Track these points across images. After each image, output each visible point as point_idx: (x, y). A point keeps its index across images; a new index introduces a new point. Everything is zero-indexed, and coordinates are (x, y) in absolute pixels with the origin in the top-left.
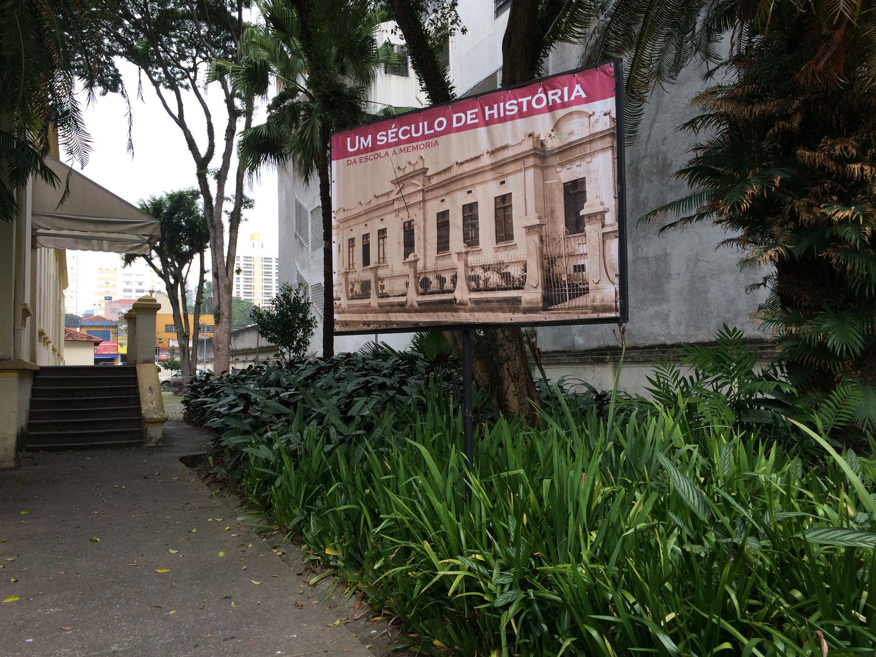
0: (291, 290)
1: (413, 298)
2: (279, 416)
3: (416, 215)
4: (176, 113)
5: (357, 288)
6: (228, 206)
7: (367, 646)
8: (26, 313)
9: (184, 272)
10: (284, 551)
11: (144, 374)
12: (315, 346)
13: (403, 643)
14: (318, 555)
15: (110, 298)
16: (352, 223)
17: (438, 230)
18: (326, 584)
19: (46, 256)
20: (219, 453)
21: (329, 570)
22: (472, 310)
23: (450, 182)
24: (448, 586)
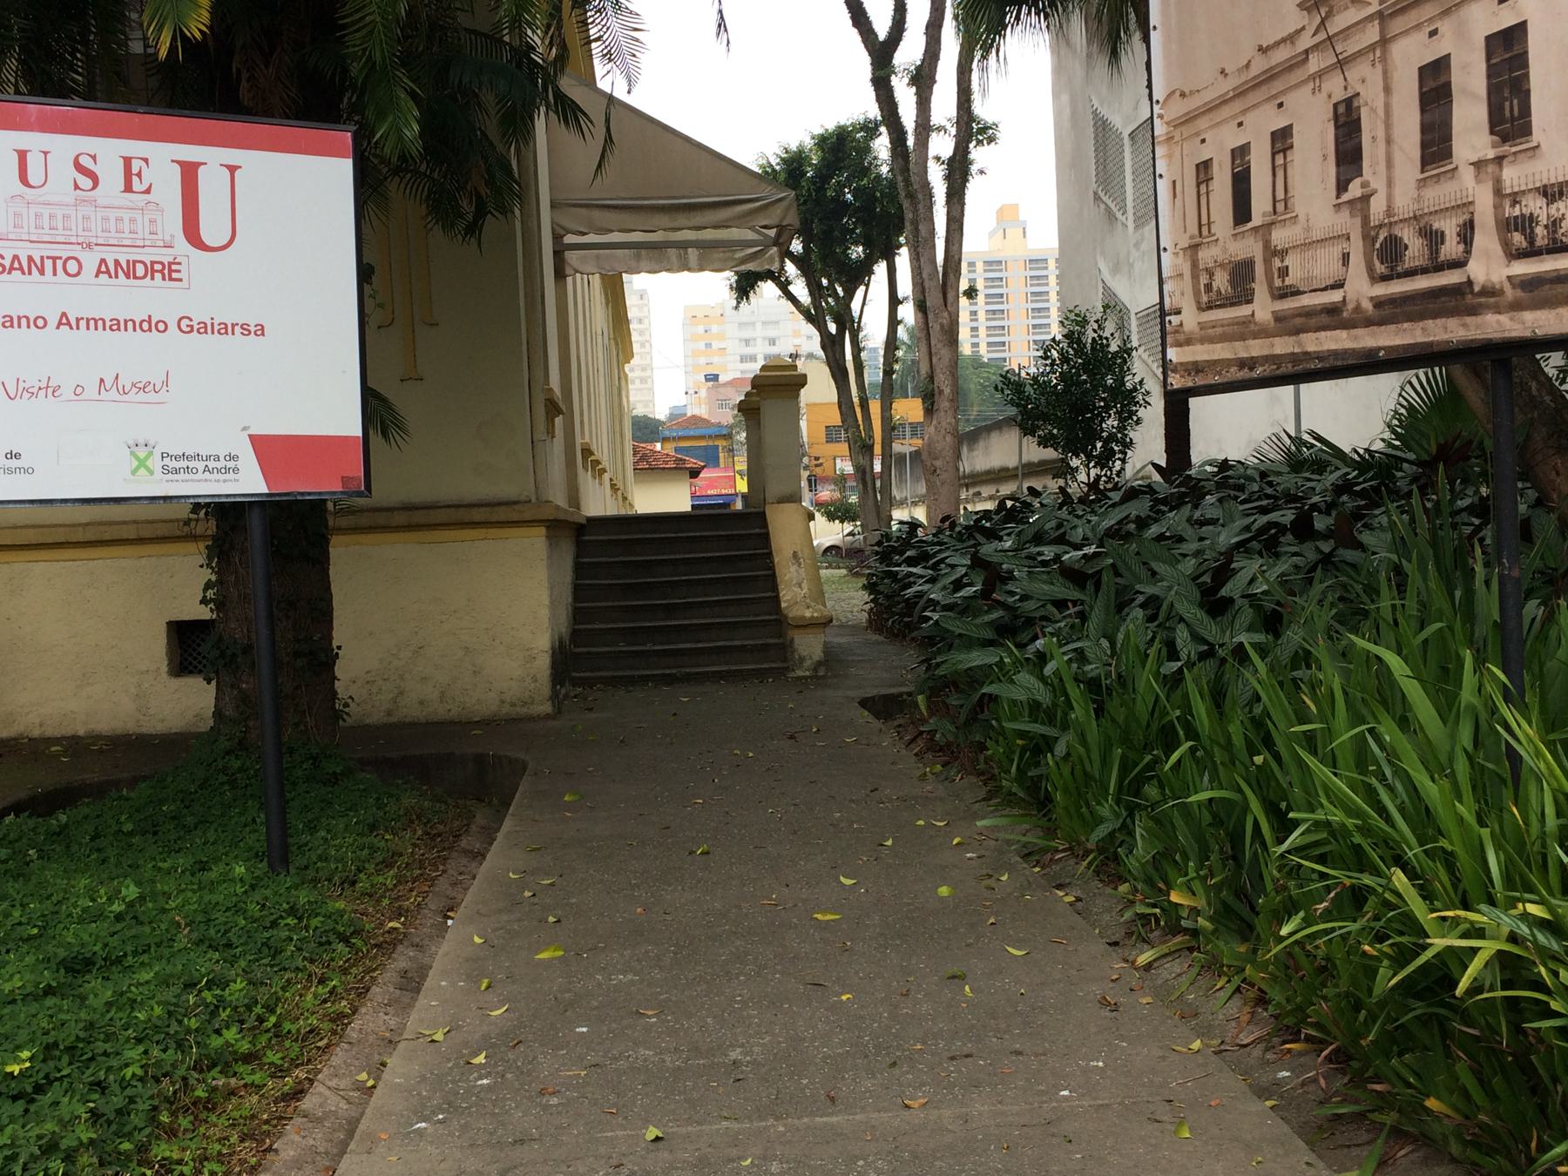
0: (1084, 322)
1: (1361, 290)
2: (1061, 604)
3: (1365, 81)
4: (882, 28)
5: (1221, 281)
6: (942, 145)
7: (1269, 1103)
8: (553, 409)
9: (856, 305)
10: (1079, 893)
11: (781, 522)
12: (1148, 445)
13: (1356, 1102)
14: (1154, 906)
15: (715, 378)
16: (1203, 123)
17: (1423, 111)
18: (1175, 966)
19: (586, 291)
20: (939, 687)
21: (1179, 939)
22: (1516, 306)
24: (1456, 976)
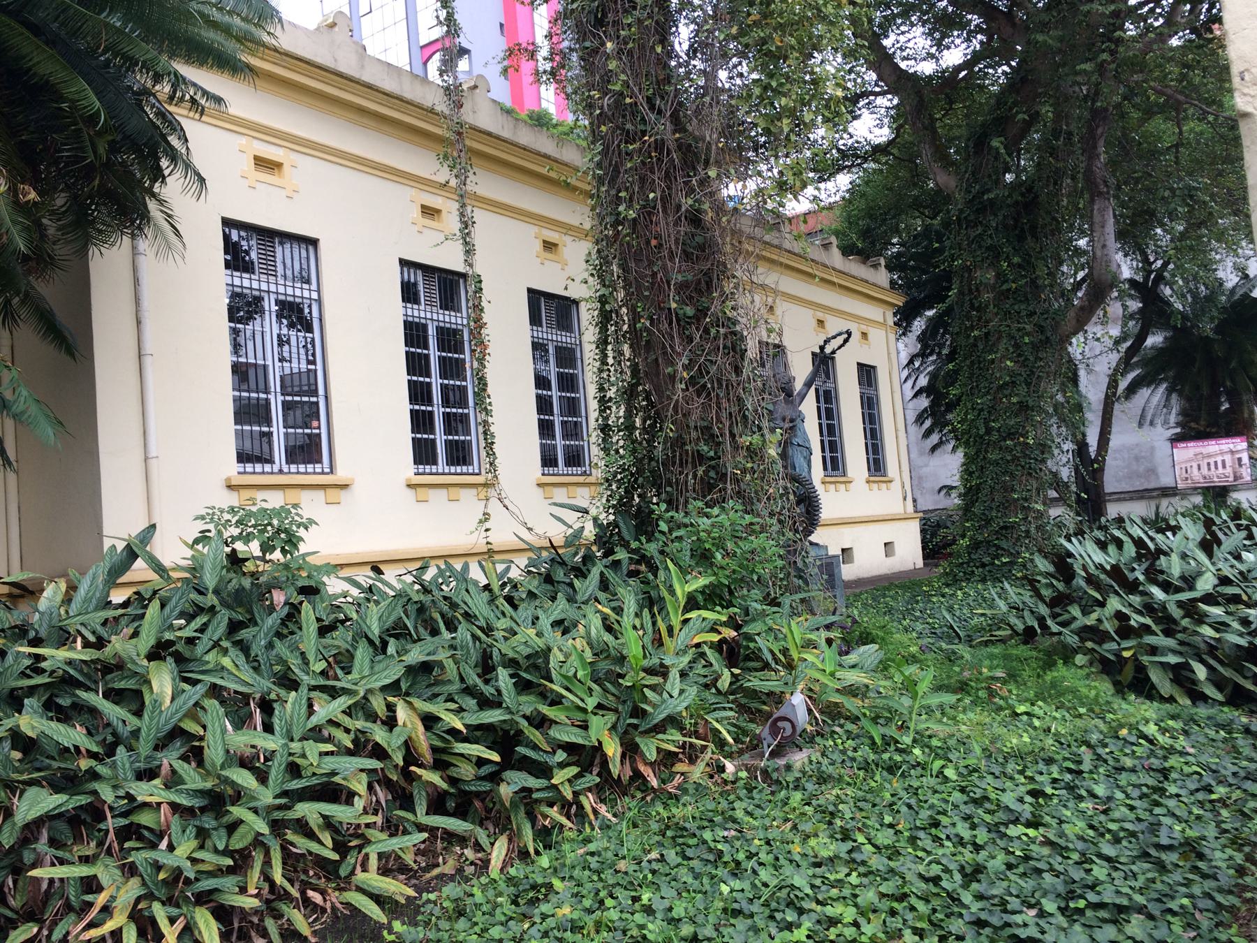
23: (1209, 456)
